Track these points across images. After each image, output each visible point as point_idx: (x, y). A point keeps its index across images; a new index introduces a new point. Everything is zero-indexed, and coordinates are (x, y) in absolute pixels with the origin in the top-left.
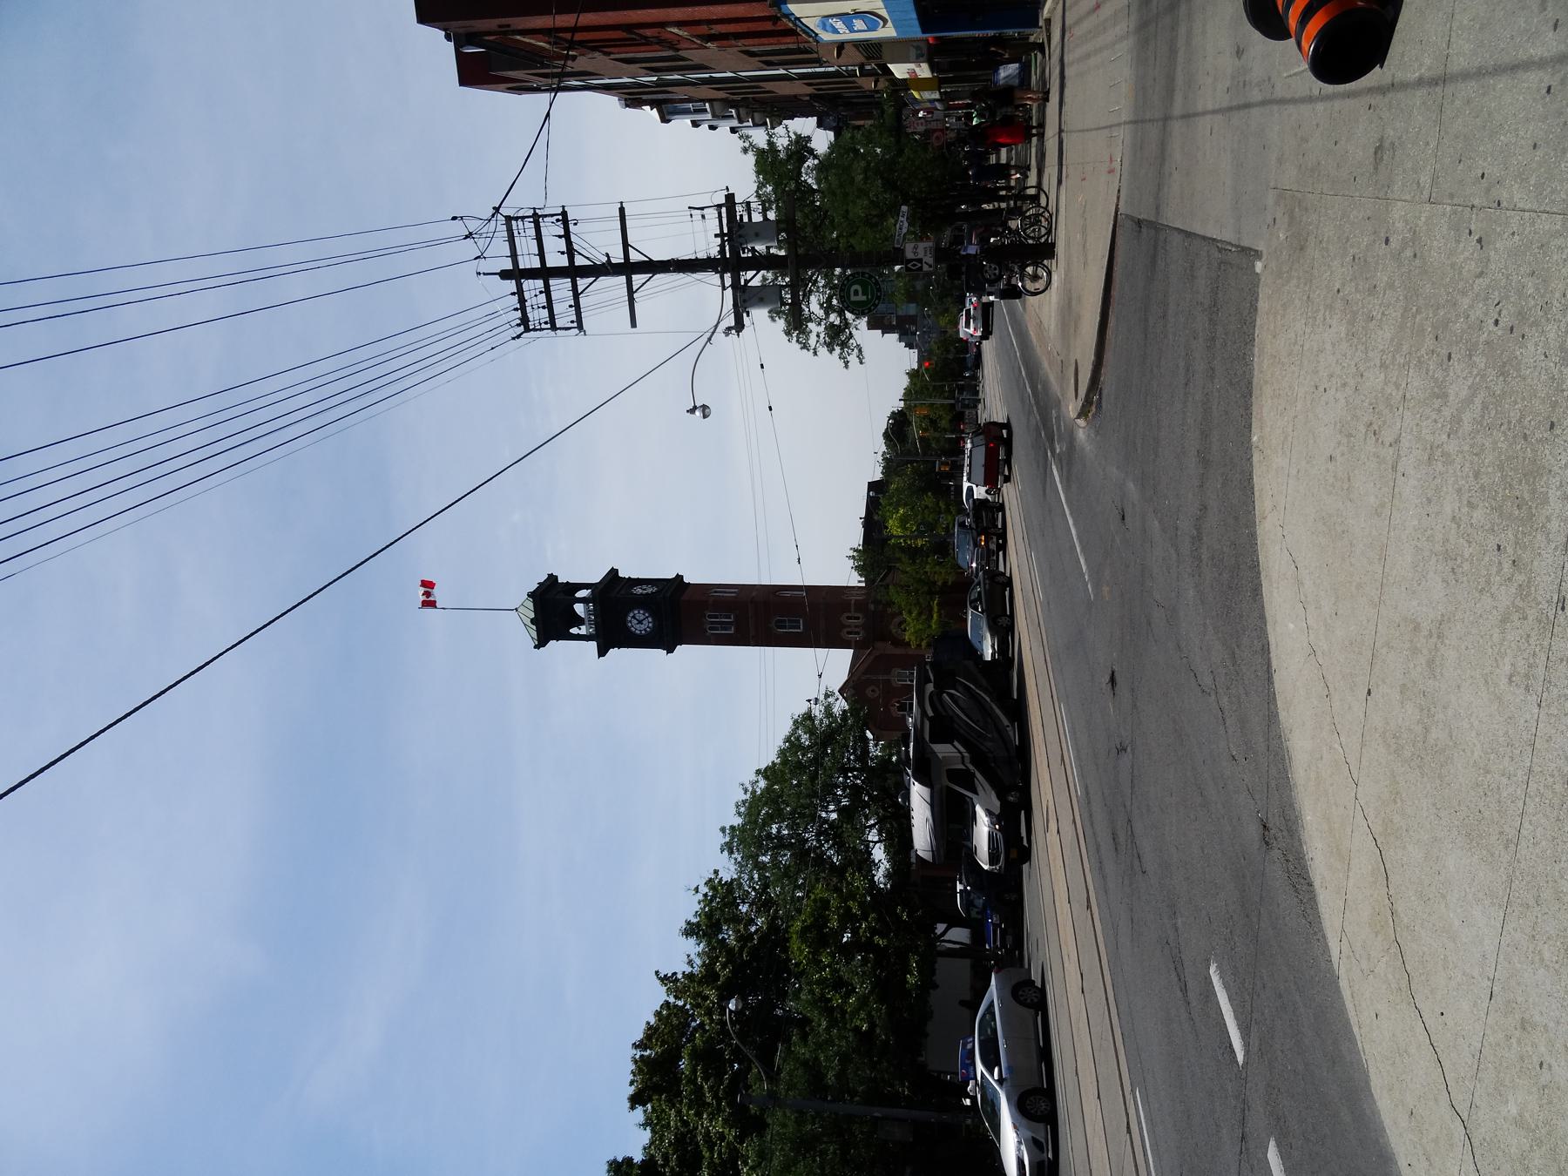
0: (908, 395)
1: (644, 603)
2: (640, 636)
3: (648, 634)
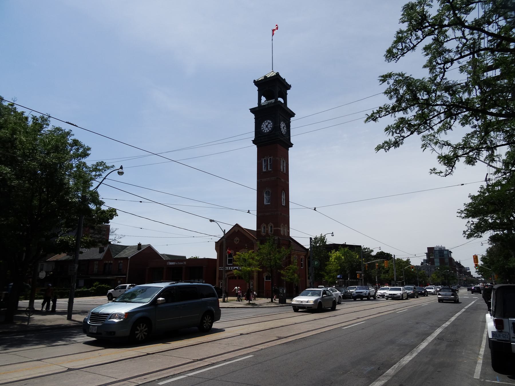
0: (399, 261)
1: (276, 128)
2: (261, 127)
3: (261, 131)
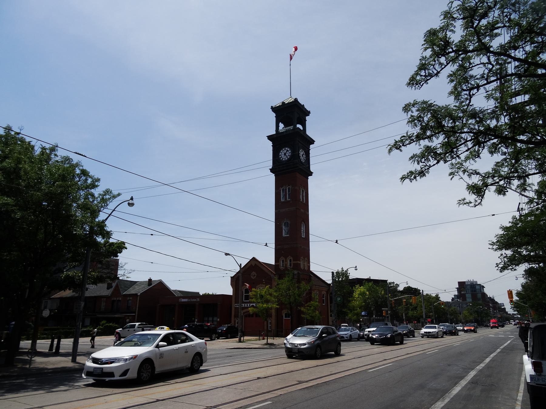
0: (428, 297)
1: (295, 156)
2: (279, 155)
3: (279, 159)
